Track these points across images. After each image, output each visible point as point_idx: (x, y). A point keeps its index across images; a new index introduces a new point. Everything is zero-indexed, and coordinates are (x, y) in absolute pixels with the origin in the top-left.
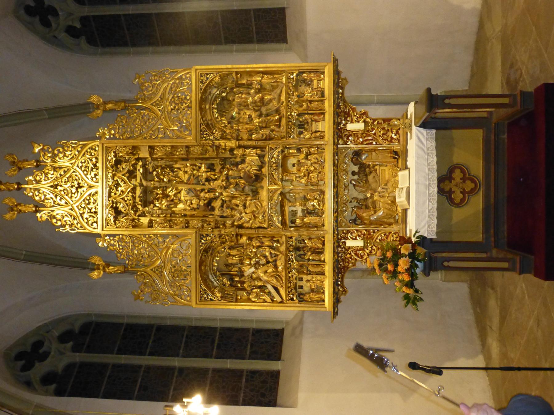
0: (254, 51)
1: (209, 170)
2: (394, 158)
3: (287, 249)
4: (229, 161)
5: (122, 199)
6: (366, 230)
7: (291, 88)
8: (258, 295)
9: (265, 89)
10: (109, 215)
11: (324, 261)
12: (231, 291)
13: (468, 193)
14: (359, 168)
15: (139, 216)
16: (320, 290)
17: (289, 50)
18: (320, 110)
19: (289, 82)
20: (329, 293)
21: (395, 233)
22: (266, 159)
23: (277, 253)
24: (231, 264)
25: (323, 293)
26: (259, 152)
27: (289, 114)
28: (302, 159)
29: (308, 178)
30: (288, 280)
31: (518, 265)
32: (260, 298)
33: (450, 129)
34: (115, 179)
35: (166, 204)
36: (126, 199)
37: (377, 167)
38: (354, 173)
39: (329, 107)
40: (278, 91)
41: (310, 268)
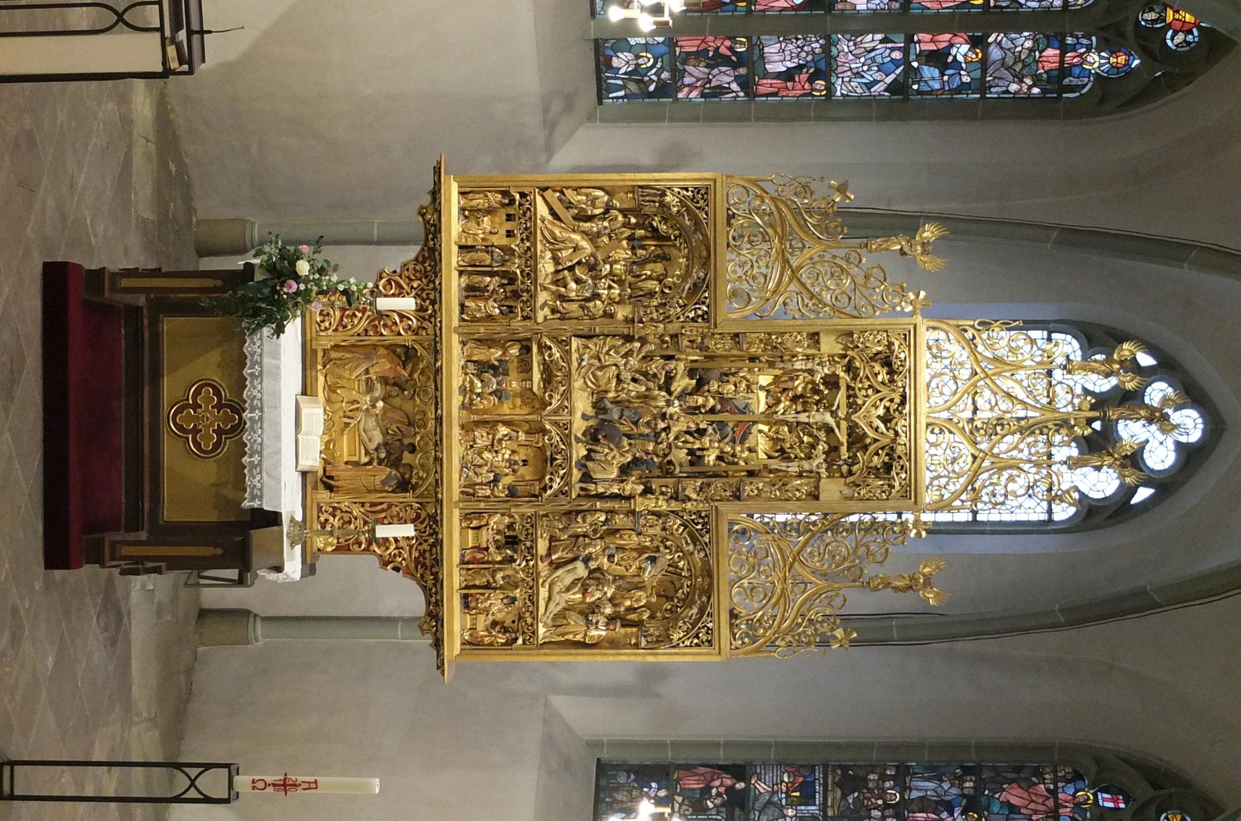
0: (676, 745)
1: (698, 453)
2: (331, 478)
3: (533, 297)
4: (650, 470)
5: (878, 392)
6: (382, 335)
7: (527, 614)
8: (593, 202)
9: (581, 613)
10: (902, 356)
11: (461, 273)
12: (649, 209)
13: (189, 406)
14: (400, 459)
15: (844, 356)
16: (468, 213)
17: (595, 745)
18: (469, 569)
19: (532, 625)
20: (450, 210)
21: (326, 329)
22: (576, 474)
23: (554, 288)
24: (655, 262)
25: (462, 209)
26: (592, 487)
27: (531, 563)
28: (507, 475)
29: (494, 436)
30: (530, 235)
31: (107, 280)
32: (587, 195)
33: (221, 525)
34: (892, 432)
35: (797, 383)
36: (870, 392)
37: (365, 460)
38: (413, 449)
39: (450, 576)
40: (554, 609)
41: (487, 259)
